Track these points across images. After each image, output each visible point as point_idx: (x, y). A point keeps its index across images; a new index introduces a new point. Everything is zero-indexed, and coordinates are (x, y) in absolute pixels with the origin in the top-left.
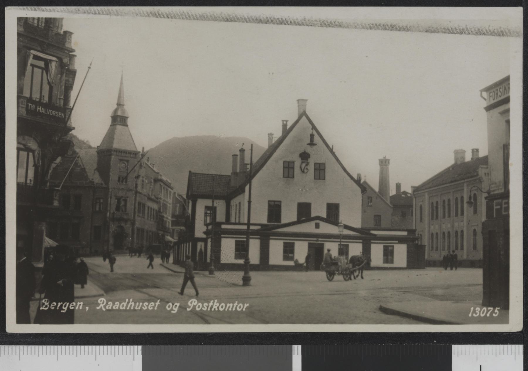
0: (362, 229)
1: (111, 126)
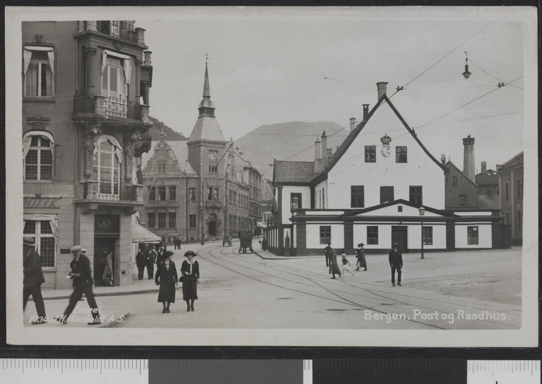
0: (445, 210)
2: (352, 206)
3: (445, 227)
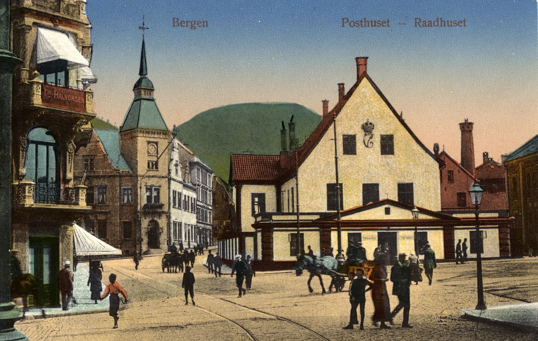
2: (328, 209)
3: (318, 233)
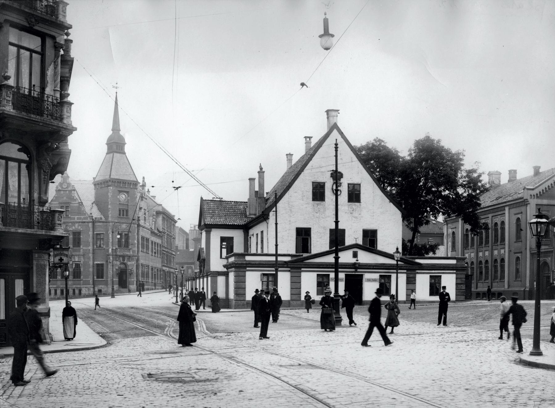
1: (107, 154)
3: (454, 276)
